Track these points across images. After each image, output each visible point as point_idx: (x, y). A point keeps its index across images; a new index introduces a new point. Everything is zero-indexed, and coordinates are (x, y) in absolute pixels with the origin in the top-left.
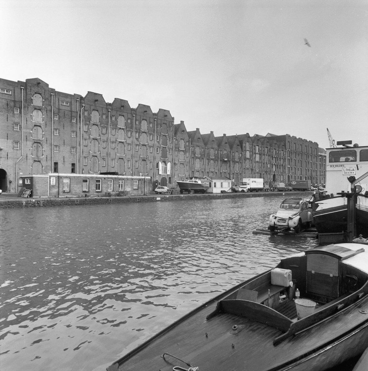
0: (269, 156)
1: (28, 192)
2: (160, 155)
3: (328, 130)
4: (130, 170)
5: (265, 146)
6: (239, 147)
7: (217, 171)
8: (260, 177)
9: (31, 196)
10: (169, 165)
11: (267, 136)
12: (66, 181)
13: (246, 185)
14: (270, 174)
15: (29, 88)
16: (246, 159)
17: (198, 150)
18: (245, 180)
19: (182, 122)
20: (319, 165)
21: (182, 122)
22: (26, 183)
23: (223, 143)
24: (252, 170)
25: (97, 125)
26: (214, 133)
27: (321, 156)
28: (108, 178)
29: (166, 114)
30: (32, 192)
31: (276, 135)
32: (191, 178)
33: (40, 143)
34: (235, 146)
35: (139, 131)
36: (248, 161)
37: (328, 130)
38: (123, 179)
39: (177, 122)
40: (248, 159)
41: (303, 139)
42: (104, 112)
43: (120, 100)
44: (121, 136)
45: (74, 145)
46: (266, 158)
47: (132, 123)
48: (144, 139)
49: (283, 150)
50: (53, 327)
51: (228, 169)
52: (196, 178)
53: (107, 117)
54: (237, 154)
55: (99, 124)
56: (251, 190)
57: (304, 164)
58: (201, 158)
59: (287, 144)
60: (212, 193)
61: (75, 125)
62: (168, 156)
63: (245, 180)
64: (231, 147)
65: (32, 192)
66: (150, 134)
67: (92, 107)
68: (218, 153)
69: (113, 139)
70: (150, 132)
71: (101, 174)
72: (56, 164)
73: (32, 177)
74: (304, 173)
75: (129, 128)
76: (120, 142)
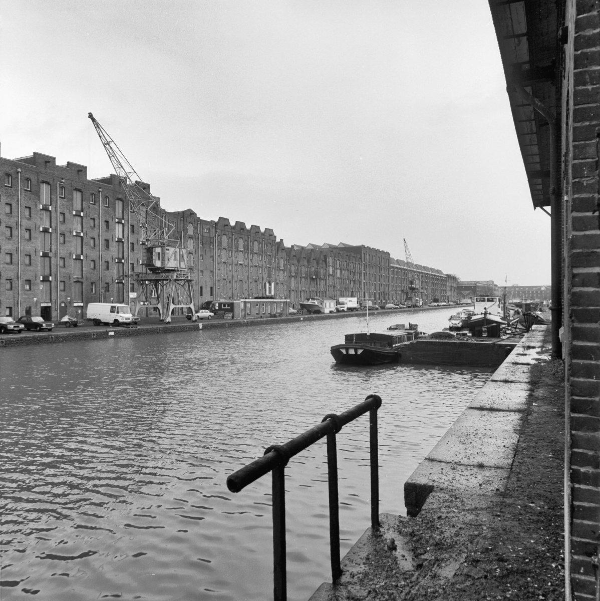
0: (348, 270)
1: (231, 315)
2: (267, 275)
3: (404, 240)
4: (247, 292)
5: (345, 260)
6: (324, 263)
7: (307, 290)
8: (352, 296)
9: (233, 317)
10: (273, 284)
11: (340, 246)
12: (248, 305)
13: (344, 304)
14: (348, 291)
15: (185, 218)
16: (329, 275)
17: (293, 268)
18: (341, 300)
19: (282, 240)
20: (391, 278)
21: (282, 240)
22: (223, 307)
23: (312, 259)
24: (334, 287)
25: (226, 249)
26: (284, 241)
27: (393, 267)
28: (268, 302)
29: (271, 233)
30: (233, 315)
31: (349, 245)
32: (308, 300)
33: (192, 269)
34: (321, 262)
35: (253, 253)
36: (331, 277)
37: (404, 240)
38: (276, 302)
39: (278, 240)
40: (331, 275)
41: (366, 246)
42: (230, 236)
43: (239, 223)
44: (240, 258)
45: (212, 269)
46: (345, 273)
47: (248, 244)
48: (256, 260)
49: (353, 263)
50: (375, 394)
51: (315, 287)
52: (313, 299)
53: (232, 240)
54: (322, 270)
55: (227, 248)
56: (350, 309)
57: (377, 277)
58: (295, 277)
59: (363, 255)
60: (324, 313)
61: (212, 250)
62: (272, 276)
63: (341, 300)
64: (318, 263)
65: (233, 315)
66: (260, 255)
67: (223, 233)
68: (308, 270)
69: (236, 262)
70: (261, 253)
71: (256, 298)
72: (201, 287)
73: (233, 303)
74: (377, 288)
75: (246, 249)
76: (240, 264)
